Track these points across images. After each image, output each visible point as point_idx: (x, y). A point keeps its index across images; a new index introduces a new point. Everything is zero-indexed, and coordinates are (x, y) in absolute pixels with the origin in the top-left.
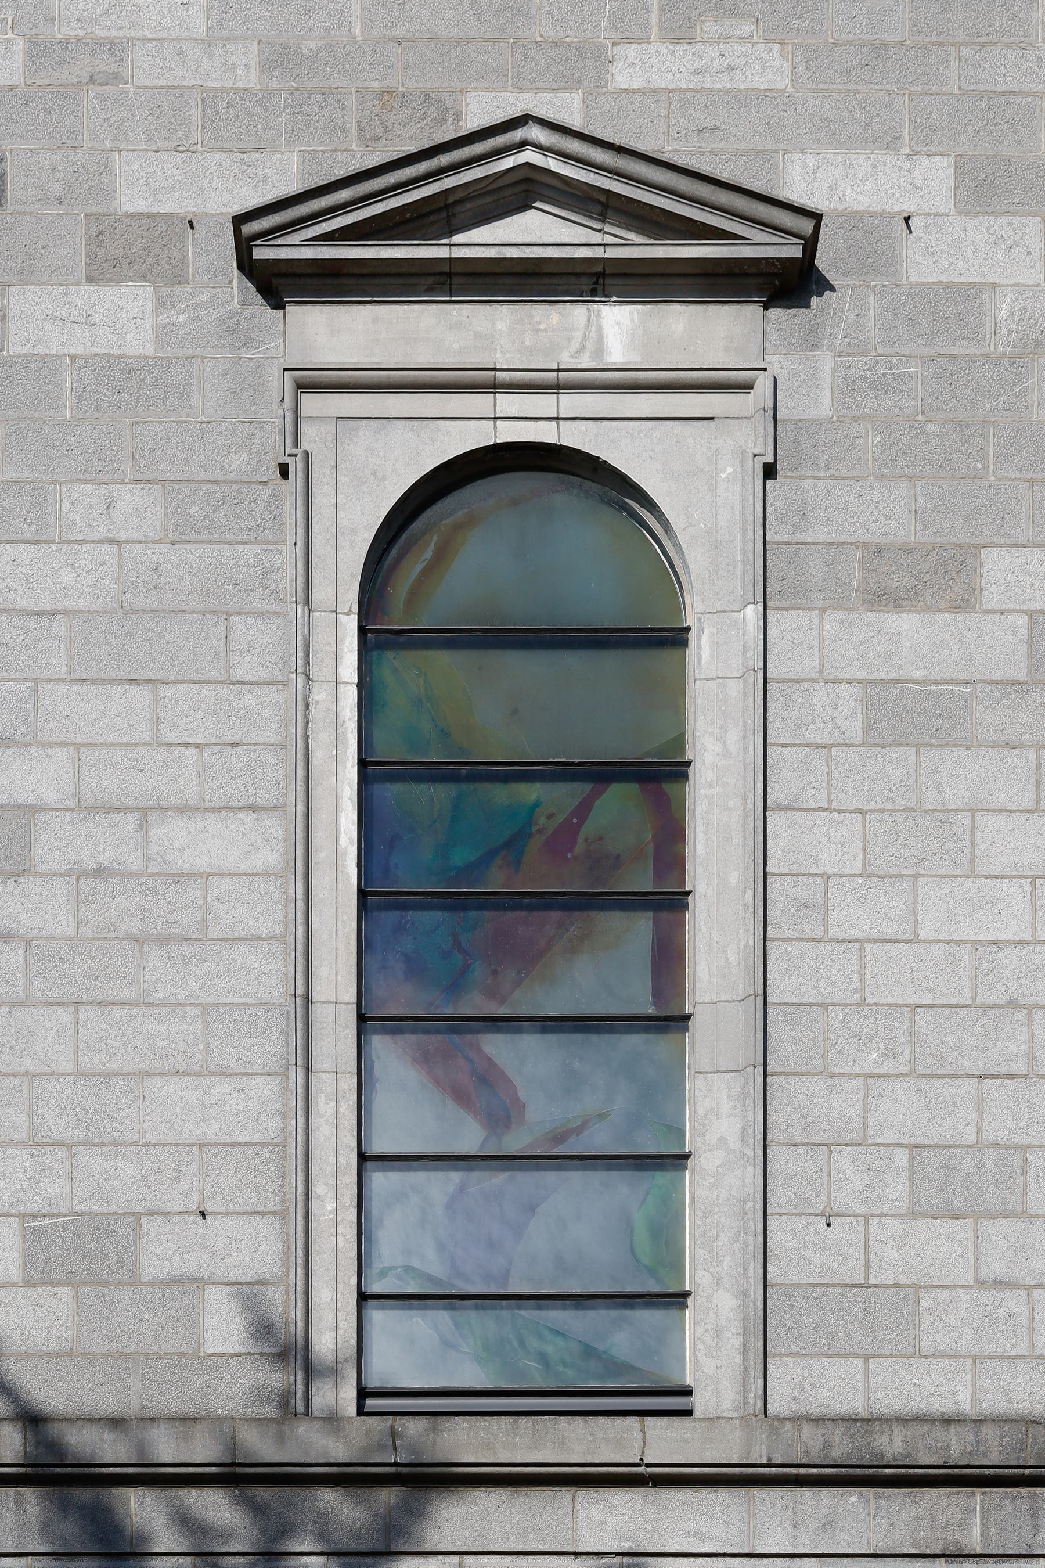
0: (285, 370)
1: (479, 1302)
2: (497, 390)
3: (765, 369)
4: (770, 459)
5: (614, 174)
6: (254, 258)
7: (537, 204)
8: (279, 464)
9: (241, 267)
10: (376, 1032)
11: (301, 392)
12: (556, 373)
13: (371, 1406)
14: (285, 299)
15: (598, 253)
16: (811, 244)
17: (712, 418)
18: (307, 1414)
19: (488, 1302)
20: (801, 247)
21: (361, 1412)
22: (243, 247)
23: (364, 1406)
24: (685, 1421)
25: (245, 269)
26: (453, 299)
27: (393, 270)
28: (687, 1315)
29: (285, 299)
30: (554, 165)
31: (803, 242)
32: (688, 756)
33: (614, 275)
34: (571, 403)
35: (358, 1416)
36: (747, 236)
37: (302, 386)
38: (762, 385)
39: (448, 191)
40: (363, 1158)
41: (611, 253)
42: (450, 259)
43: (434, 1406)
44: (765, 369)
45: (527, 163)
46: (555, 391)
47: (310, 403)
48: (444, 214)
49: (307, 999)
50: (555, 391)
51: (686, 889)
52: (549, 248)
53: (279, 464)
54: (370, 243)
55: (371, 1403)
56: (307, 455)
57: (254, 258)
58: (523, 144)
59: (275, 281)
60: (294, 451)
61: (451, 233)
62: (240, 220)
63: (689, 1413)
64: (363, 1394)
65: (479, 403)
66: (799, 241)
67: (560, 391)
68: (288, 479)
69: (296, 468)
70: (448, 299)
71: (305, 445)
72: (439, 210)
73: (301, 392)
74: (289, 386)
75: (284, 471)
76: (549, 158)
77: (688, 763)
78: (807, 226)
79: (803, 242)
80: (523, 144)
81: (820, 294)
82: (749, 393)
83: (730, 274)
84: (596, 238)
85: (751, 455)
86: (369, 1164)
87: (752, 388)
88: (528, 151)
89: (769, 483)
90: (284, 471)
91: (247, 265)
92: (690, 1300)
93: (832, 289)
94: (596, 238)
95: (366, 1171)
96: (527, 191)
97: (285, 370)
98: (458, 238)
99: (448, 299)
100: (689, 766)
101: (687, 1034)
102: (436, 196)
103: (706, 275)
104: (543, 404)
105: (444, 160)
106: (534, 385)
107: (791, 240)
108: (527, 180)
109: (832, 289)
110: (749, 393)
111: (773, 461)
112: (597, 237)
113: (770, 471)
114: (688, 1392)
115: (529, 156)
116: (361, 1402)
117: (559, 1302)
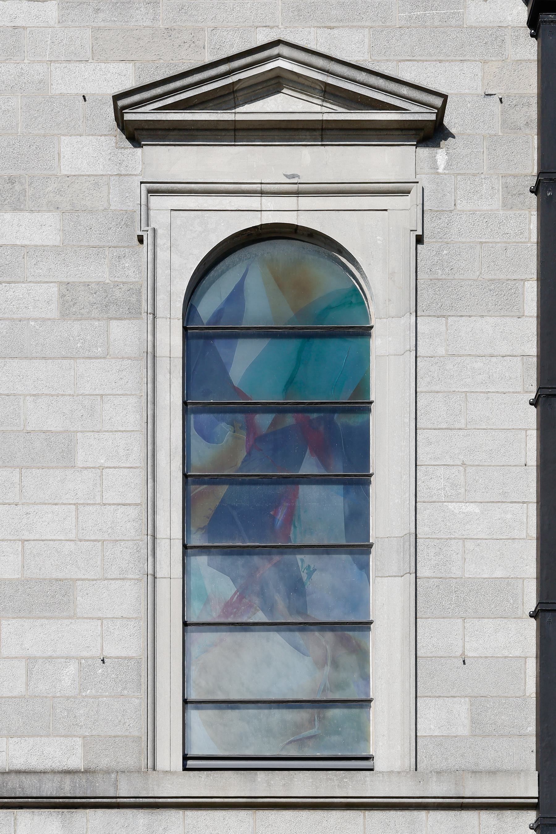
0: (141, 183)
1: (219, 705)
2: (299, 195)
3: (418, 182)
6: (125, 119)
11: (150, 196)
13: (190, 765)
14: (143, 143)
15: (319, 117)
16: (441, 112)
17: (386, 210)
18: (154, 769)
19: (203, 705)
20: (435, 114)
21: (185, 769)
22: (119, 113)
23: (186, 765)
26: (236, 143)
27: (283, 126)
29: (143, 143)
31: (436, 111)
33: (243, 129)
34: (306, 202)
35: (183, 770)
36: (406, 108)
38: (416, 190)
39: (233, 83)
41: (326, 117)
43: (198, 765)
44: (418, 182)
46: (260, 195)
47: (155, 201)
48: (232, 97)
49: (154, 537)
50: (260, 195)
52: (249, 115)
54: (188, 111)
55: (191, 763)
56: (154, 230)
57: (125, 119)
58: (279, 56)
59: (136, 133)
60: (146, 228)
61: (235, 107)
62: (116, 98)
63: (372, 770)
64: (186, 758)
65: (253, 202)
67: (263, 195)
68: (143, 244)
69: (148, 239)
70: (233, 143)
71: (153, 225)
72: (229, 94)
73: (150, 196)
74: (144, 193)
75: (141, 240)
78: (438, 102)
79: (436, 111)
80: (279, 56)
81: (446, 139)
82: (408, 196)
83: (279, 129)
84: (318, 109)
86: (189, 628)
88: (280, 60)
89: (419, 246)
90: (141, 240)
92: (372, 703)
93: (454, 137)
94: (318, 109)
95: (187, 632)
97: (141, 183)
98: (238, 110)
99: (233, 143)
103: (401, 130)
106: (253, 191)
108: (278, 77)
109: (454, 137)
110: (408, 196)
111: (421, 234)
112: (325, 110)
113: (419, 240)
117: (253, 705)
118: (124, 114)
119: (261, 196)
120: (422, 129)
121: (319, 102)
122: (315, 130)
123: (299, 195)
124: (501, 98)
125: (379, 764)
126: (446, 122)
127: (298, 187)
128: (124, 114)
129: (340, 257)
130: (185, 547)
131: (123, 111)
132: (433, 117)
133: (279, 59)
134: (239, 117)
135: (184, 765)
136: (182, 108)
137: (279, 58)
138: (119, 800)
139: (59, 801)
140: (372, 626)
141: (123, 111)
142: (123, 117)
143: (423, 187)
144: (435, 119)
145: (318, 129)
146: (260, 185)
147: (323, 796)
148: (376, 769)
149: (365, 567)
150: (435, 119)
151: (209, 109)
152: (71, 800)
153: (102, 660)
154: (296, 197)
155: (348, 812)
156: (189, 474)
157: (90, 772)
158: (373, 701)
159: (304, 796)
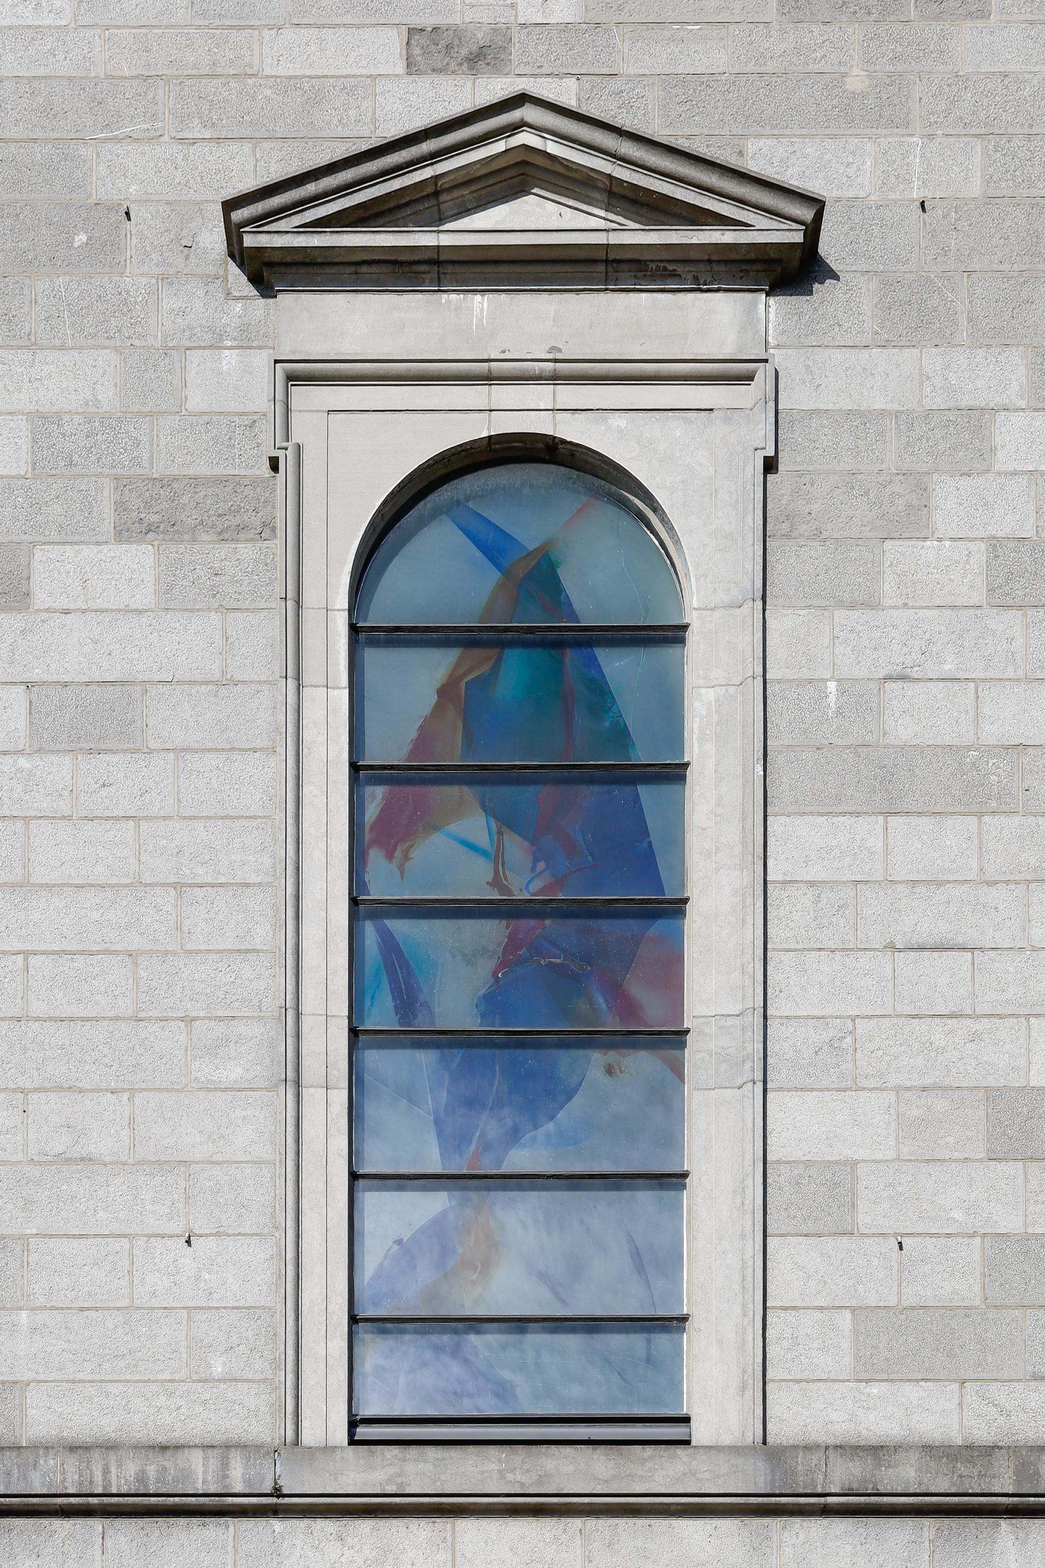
0: (276, 362)
2: (492, 382)
3: (766, 361)
4: (771, 453)
5: (618, 160)
7: (535, 190)
8: (269, 457)
9: (231, 255)
10: (370, 1046)
11: (292, 385)
12: (553, 364)
16: (813, 231)
17: (711, 410)
21: (352, 1442)
22: (233, 233)
24: (680, 1450)
25: (236, 258)
28: (685, 1196)
30: (553, 148)
31: (804, 228)
32: (686, 1025)
34: (570, 395)
37: (292, 378)
40: (354, 1177)
41: (615, 239)
42: (438, 246)
43: (381, 1434)
44: (766, 361)
45: (524, 145)
51: (685, 1027)
53: (269, 457)
55: (363, 1432)
56: (299, 448)
60: (285, 444)
62: (230, 206)
63: (687, 1443)
64: (353, 1423)
66: (795, 226)
70: (437, 288)
71: (296, 437)
73: (292, 385)
75: (274, 464)
76: (548, 141)
77: (686, 765)
78: (807, 214)
82: (750, 384)
84: (594, 223)
85: (752, 449)
86: (361, 1183)
87: (753, 381)
88: (524, 133)
91: (238, 253)
93: (835, 277)
96: (523, 174)
97: (276, 362)
99: (437, 288)
100: (686, 903)
101: (685, 1191)
102: (711, 213)
104: (541, 395)
105: (311, 188)
107: (789, 225)
108: (524, 163)
110: (750, 384)
113: (770, 465)
114: (686, 1420)
115: (526, 138)
116: (353, 1430)
118: (244, 235)
119: (490, 385)
120: (779, 261)
121: (602, 213)
122: (594, 261)
123: (492, 382)
124: (923, 202)
125: (701, 1432)
126: (823, 249)
127: (489, 367)
128: (244, 235)
129: (632, 498)
130: (354, 1032)
131: (241, 230)
132: (798, 238)
133: (523, 131)
134: (446, 240)
135: (351, 1433)
136: (347, 222)
137: (524, 128)
138: (230, 1500)
139: (1039, 1501)
140: (687, 1181)
141: (241, 230)
142: (241, 241)
143: (776, 369)
144: (802, 241)
145: (601, 261)
146: (551, 364)
147: (707, 1492)
148: (693, 1443)
149: (678, 1070)
150: (802, 241)
151: (433, 225)
152: (59, 1500)
153: (186, 1242)
154: (552, 386)
155: (766, 1521)
156: (361, 898)
157: (189, 1447)
158: (690, 1319)
159: (605, 1492)
